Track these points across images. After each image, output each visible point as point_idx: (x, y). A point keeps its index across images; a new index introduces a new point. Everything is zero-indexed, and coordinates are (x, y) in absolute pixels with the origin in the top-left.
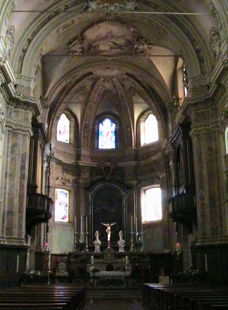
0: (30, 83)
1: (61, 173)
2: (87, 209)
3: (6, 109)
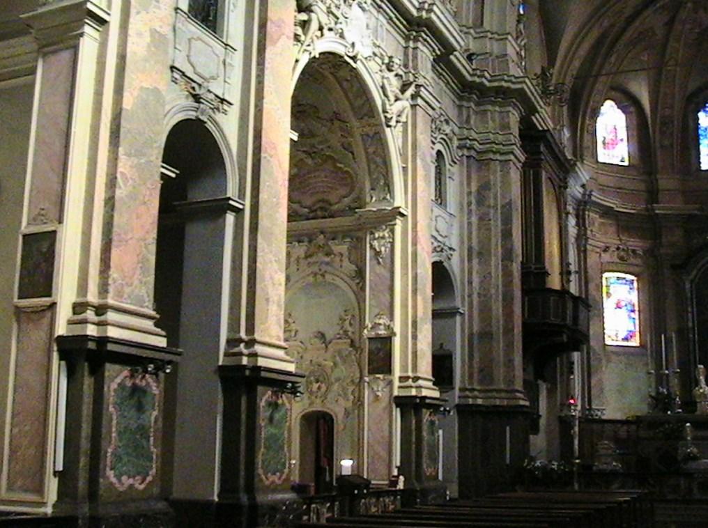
0: (505, 45)
1: (616, 237)
2: (681, 316)
3: (456, 111)
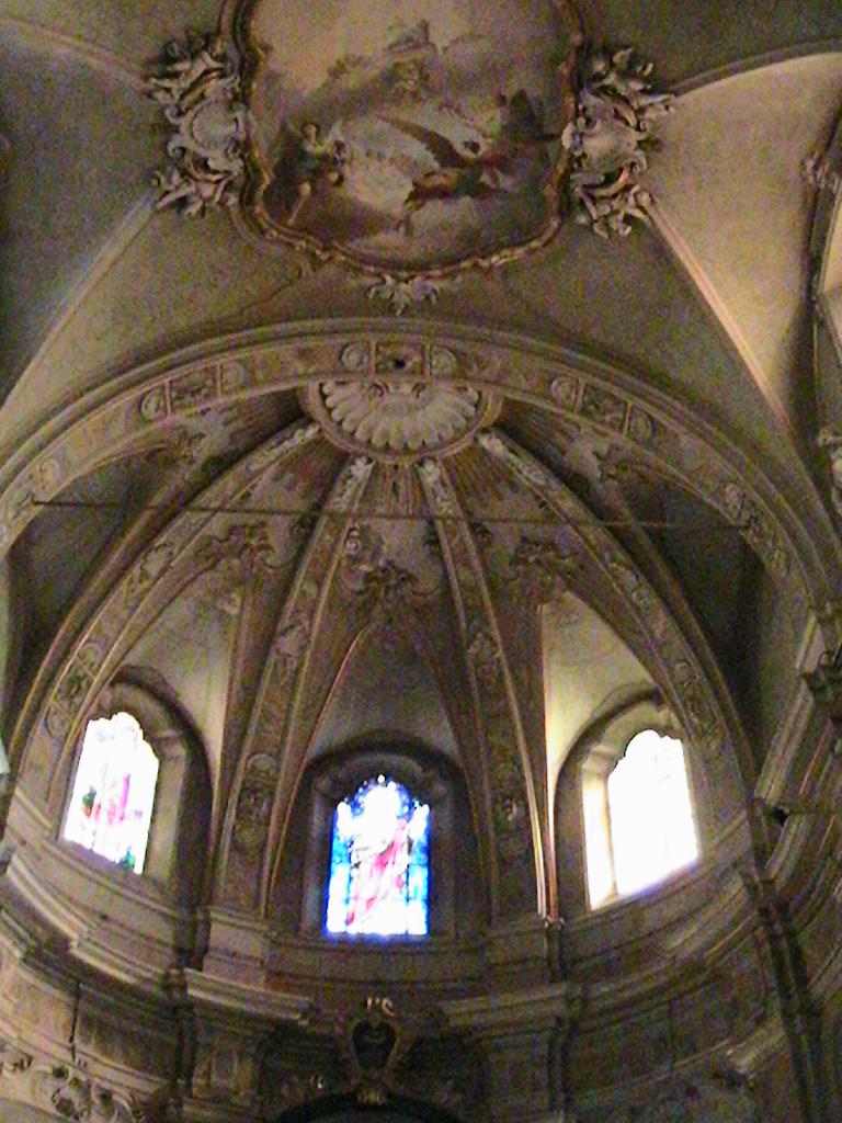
1: (62, 1038)
